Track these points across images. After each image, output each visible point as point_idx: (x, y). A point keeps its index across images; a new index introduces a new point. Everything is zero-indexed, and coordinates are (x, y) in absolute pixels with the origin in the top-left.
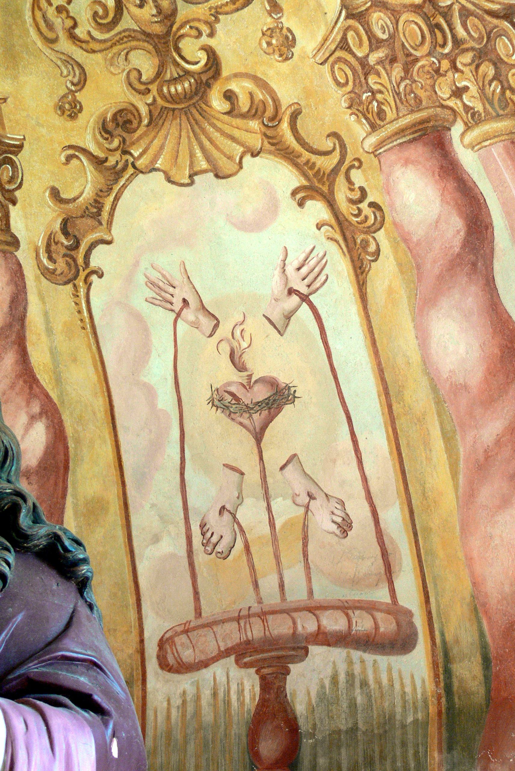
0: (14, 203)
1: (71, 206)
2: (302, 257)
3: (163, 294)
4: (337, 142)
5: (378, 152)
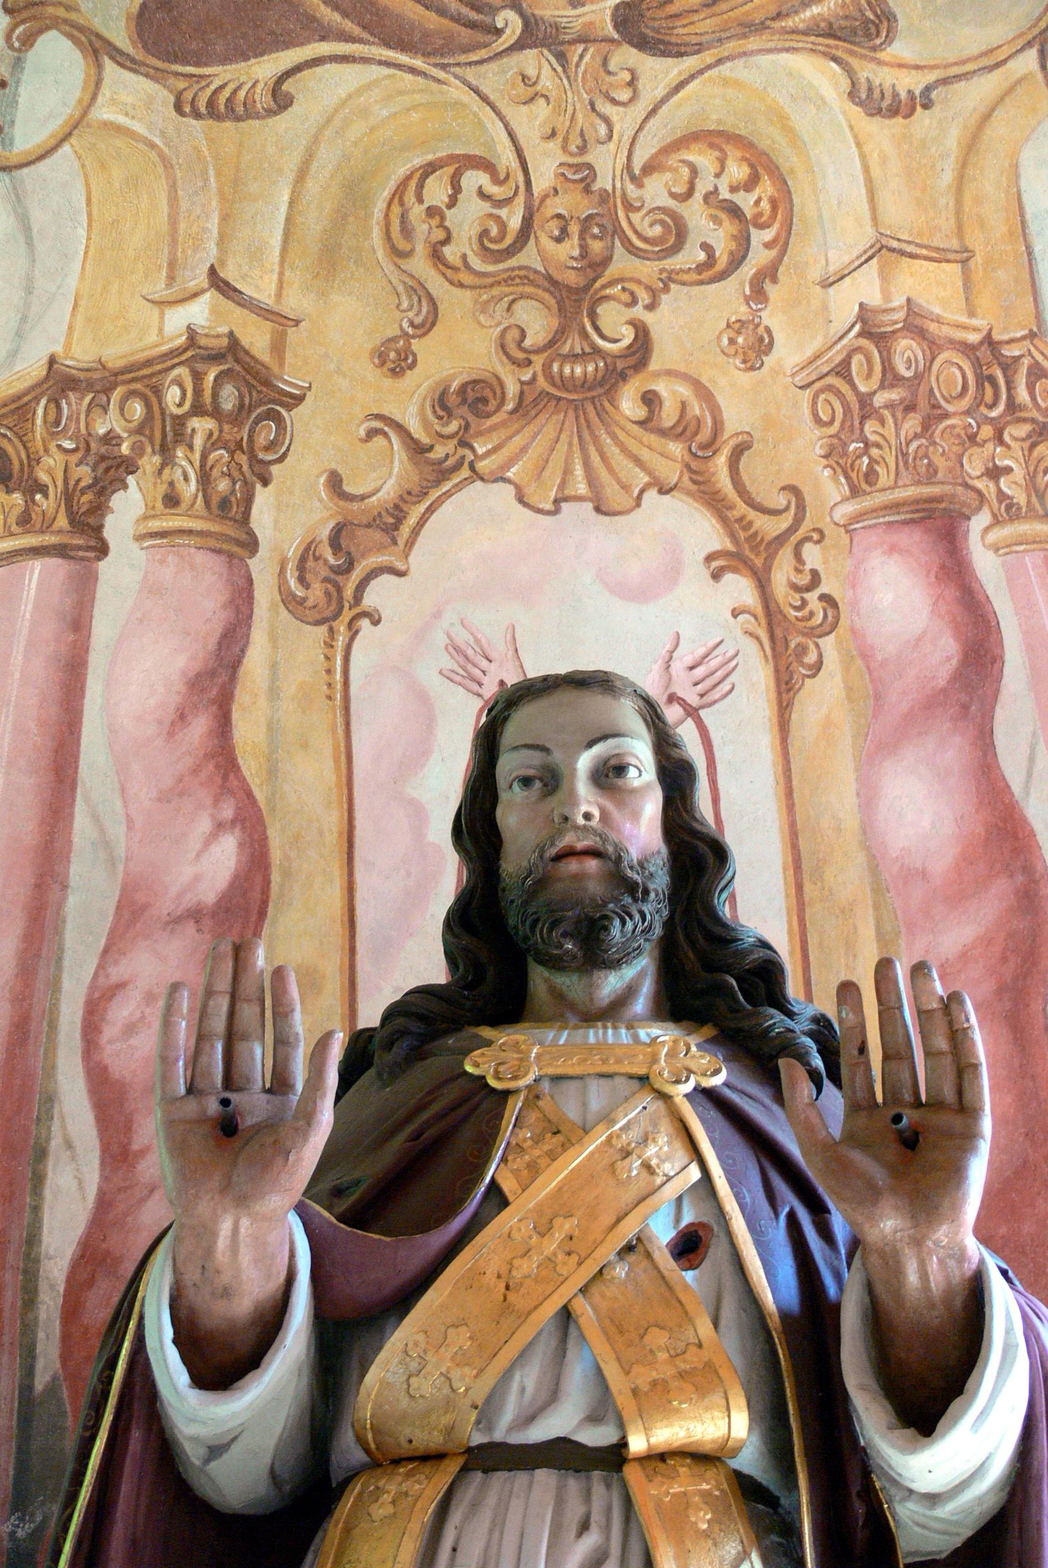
0: (266, 482)
1: (355, 506)
2: (702, 651)
3: (470, 667)
4: (794, 500)
5: (853, 527)
